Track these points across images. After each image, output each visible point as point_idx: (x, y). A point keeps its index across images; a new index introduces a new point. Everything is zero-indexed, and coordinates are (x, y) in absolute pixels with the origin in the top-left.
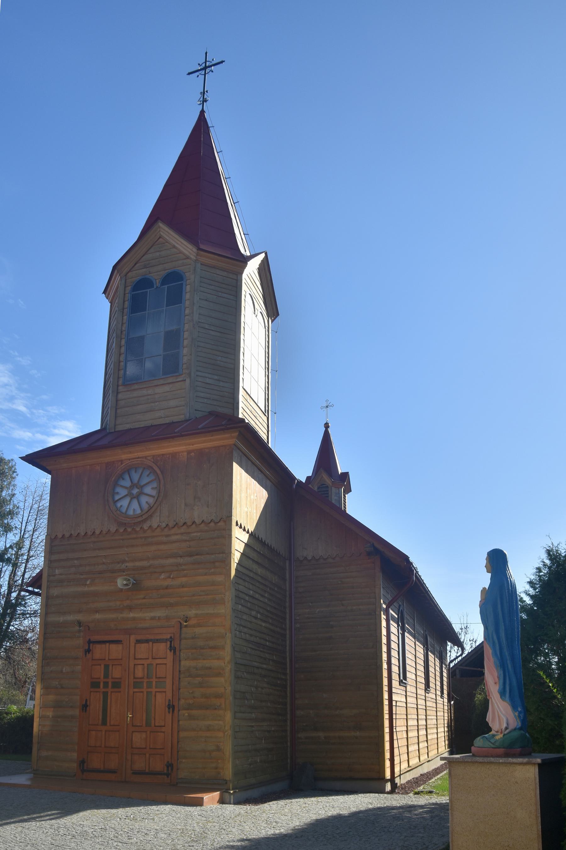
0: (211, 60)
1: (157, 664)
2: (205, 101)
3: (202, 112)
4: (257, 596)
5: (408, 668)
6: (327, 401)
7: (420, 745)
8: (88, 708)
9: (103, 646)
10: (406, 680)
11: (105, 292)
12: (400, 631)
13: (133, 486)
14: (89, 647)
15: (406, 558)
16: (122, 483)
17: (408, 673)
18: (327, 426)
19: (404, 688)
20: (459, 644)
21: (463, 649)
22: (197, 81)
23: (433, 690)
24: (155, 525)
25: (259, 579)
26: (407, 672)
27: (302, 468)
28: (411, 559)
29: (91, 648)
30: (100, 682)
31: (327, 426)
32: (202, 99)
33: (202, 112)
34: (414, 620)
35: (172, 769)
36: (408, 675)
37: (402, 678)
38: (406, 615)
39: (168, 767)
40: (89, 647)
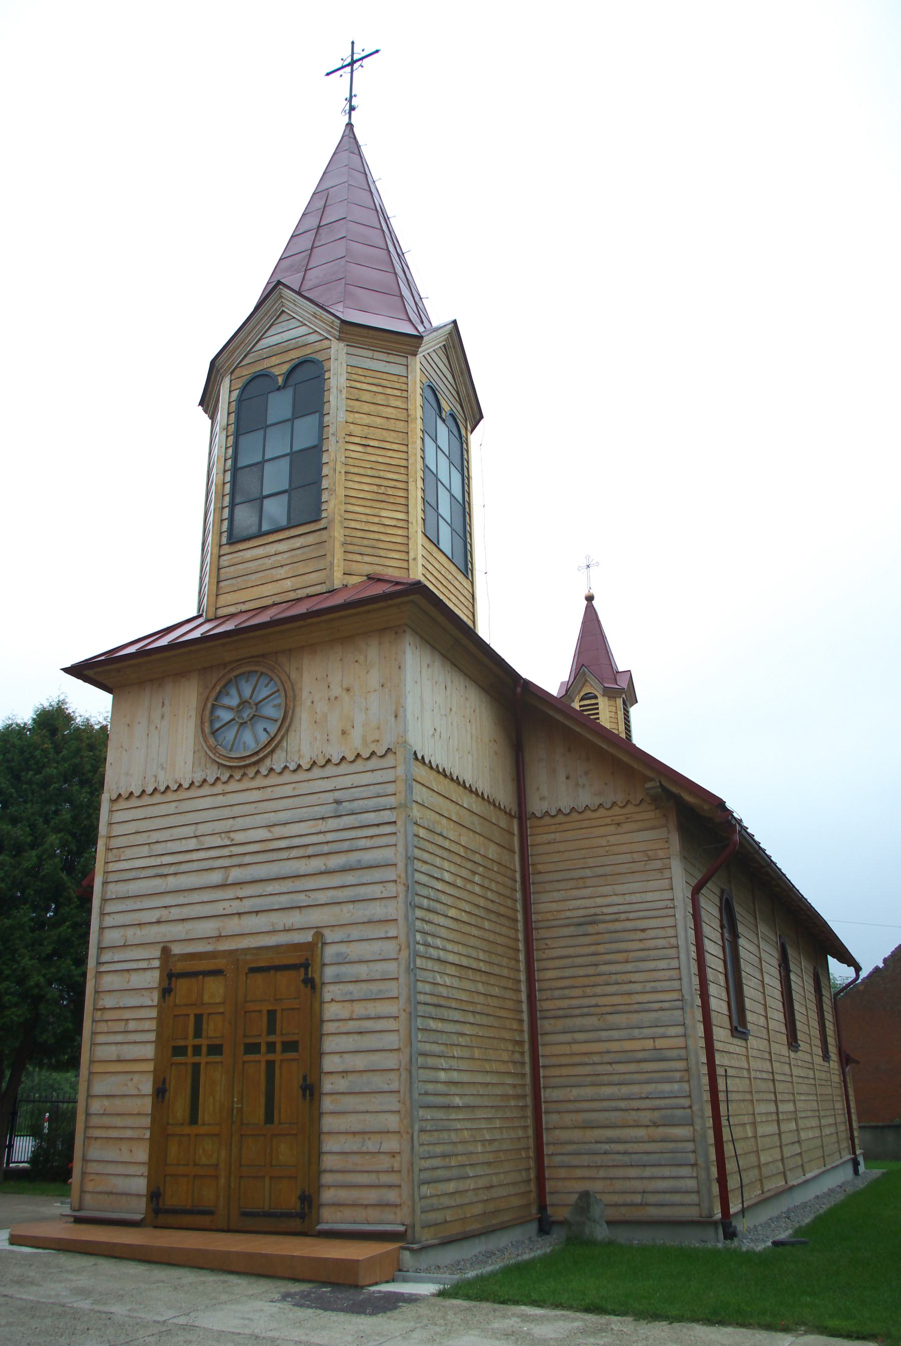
0: (360, 51)
1: (209, 1014)
2: (352, 108)
3: (350, 125)
4: (459, 882)
5: (748, 1004)
6: (588, 557)
7: (785, 1149)
8: (167, 1094)
9: (194, 980)
10: (745, 1026)
11: (201, 403)
12: (726, 935)
13: (243, 703)
14: (170, 984)
15: (721, 804)
16: (226, 701)
17: (748, 1014)
18: (590, 598)
19: (743, 1043)
20: (846, 958)
21: (858, 969)
22: (341, 82)
23: (803, 1046)
24: (278, 768)
25: (462, 852)
26: (747, 1012)
27: (546, 665)
28: (729, 805)
29: (173, 986)
30: (259, 1044)
31: (590, 598)
32: (347, 108)
33: (350, 125)
34: (756, 918)
35: (310, 1207)
36: (750, 1017)
37: (735, 1024)
38: (737, 909)
39: (302, 1203)
40: (170, 984)
